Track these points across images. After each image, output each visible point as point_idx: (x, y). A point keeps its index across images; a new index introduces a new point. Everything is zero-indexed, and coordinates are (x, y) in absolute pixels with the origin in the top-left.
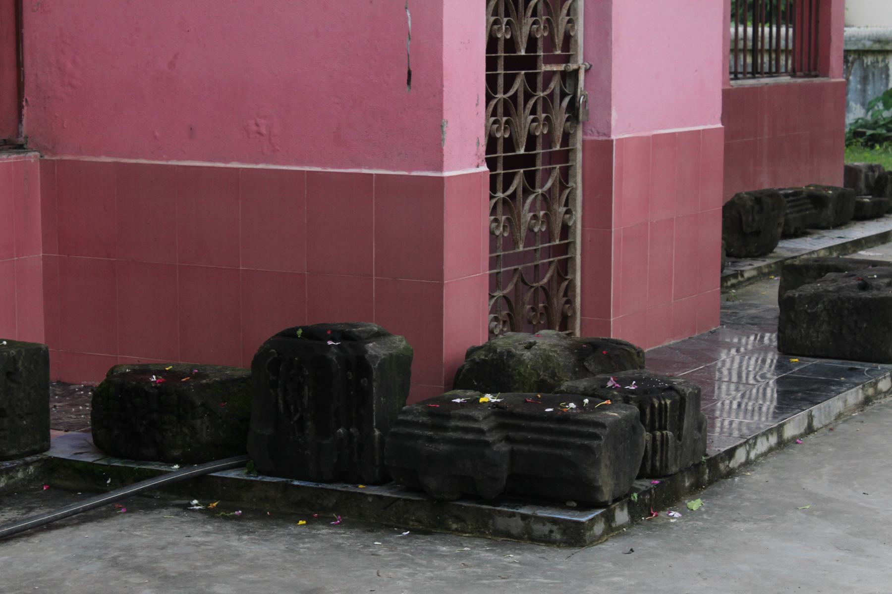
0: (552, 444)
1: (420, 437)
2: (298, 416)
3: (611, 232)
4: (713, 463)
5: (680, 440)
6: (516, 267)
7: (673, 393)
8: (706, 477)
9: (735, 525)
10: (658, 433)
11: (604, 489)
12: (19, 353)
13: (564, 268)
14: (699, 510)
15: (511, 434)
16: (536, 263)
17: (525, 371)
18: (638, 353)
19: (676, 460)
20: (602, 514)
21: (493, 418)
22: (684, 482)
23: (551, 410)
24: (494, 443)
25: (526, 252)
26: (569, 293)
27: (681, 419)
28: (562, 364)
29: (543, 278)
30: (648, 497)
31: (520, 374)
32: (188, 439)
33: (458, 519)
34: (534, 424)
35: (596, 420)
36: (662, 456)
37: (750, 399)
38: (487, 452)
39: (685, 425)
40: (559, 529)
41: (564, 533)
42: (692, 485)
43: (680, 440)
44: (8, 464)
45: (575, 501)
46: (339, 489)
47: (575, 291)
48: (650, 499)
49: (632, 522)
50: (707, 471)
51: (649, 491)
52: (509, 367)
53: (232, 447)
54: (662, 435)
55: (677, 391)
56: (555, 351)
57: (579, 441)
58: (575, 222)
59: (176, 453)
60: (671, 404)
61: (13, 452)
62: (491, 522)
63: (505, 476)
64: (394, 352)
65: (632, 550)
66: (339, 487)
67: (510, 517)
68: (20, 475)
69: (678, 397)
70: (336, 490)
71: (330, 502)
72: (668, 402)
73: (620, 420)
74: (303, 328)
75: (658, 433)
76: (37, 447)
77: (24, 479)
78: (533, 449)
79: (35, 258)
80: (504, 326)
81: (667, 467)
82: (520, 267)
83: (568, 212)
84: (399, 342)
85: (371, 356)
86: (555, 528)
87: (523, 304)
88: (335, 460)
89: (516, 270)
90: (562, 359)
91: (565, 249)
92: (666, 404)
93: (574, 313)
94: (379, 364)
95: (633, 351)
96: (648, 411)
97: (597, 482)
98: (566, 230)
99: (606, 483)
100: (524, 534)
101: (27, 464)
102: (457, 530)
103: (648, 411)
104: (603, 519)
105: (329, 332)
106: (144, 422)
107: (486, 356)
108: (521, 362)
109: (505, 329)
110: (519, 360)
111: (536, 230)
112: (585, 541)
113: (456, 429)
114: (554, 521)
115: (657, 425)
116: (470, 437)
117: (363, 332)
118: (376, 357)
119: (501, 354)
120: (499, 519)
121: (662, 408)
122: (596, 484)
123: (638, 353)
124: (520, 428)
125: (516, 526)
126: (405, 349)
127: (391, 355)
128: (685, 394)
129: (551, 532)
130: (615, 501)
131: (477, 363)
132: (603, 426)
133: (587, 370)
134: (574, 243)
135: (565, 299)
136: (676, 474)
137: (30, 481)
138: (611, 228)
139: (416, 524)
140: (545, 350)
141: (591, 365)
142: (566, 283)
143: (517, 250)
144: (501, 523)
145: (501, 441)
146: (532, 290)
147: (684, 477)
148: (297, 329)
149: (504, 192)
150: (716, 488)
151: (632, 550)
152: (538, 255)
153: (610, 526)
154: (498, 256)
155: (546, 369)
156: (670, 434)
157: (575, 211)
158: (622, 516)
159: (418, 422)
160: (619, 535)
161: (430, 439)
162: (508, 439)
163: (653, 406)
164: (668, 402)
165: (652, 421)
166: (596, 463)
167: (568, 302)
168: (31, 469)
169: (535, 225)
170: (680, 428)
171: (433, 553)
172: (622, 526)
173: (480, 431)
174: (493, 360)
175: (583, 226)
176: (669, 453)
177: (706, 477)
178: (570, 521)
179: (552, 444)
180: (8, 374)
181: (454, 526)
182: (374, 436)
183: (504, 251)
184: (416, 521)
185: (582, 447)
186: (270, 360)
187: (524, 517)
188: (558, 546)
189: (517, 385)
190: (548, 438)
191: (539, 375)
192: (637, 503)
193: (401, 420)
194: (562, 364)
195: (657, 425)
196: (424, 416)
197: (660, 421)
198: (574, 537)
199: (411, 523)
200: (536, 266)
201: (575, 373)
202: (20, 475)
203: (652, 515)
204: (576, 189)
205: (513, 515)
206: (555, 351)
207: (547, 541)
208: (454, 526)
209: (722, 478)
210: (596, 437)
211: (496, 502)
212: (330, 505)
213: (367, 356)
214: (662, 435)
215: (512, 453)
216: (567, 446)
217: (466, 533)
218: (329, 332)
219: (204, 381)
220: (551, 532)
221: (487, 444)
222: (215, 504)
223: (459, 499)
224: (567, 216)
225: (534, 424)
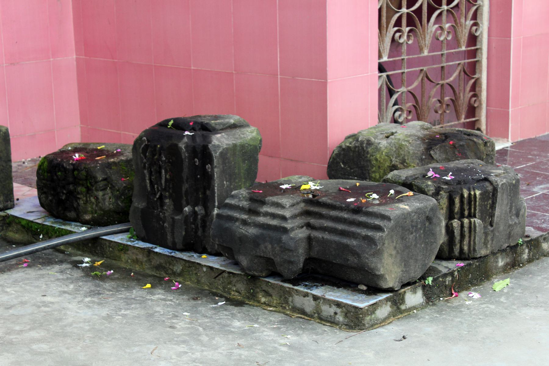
0: (343, 233)
1: (237, 219)
2: (159, 194)
3: (510, 40)
4: (534, 244)
5: (492, 226)
6: (421, 68)
7: (487, 184)
8: (525, 256)
9: (525, 310)
10: (466, 221)
11: (387, 276)
13: (472, 69)
14: (502, 291)
15: (313, 221)
16: (442, 65)
17: (380, 157)
18: (485, 144)
19: (485, 244)
20: (387, 299)
21: (302, 205)
22: (497, 262)
23: (352, 200)
24: (292, 229)
25: (430, 56)
26: (477, 89)
27: (493, 206)
28: (411, 152)
29: (451, 77)
30: (449, 279)
31: (376, 160)
32: (94, 206)
33: (267, 294)
34: (333, 213)
35: (383, 213)
36: (470, 241)
37: (462, 216)
38: (284, 238)
39: (497, 212)
40: (342, 312)
41: (346, 316)
42: (507, 265)
43: (492, 226)
45: (365, 285)
46: (185, 258)
47: (481, 87)
48: (452, 281)
49: (427, 303)
50: (527, 251)
51: (452, 274)
52: (368, 153)
53: (118, 216)
54: (470, 222)
55: (491, 183)
56: (408, 141)
57: (364, 232)
58: (482, 33)
59: (87, 217)
60: (481, 194)
62: (290, 299)
63: (302, 259)
64: (238, 142)
65: (404, 337)
66: (184, 256)
67: (304, 297)
69: (490, 188)
70: (182, 259)
71: (178, 268)
72: (478, 193)
73: (409, 214)
74: (175, 120)
75: (466, 221)
78: (327, 236)
79: (70, 59)
80: (408, 115)
81: (474, 250)
82: (425, 68)
83: (476, 24)
84: (250, 134)
85: (214, 145)
86: (339, 310)
87: (430, 97)
88: (184, 233)
89: (422, 70)
90: (414, 148)
91: (473, 54)
92: (475, 194)
93: (480, 104)
94: (221, 153)
95: (480, 142)
96: (457, 201)
97: (379, 271)
98: (473, 39)
99: (390, 270)
100: (315, 313)
102: (265, 303)
103: (457, 201)
104: (389, 303)
105: (191, 124)
106: (65, 192)
107: (350, 144)
108: (377, 149)
109: (410, 118)
110: (376, 148)
111: (442, 39)
112: (364, 325)
113: (266, 214)
114: (339, 305)
115: (466, 213)
116: (274, 222)
117: (220, 124)
118: (218, 146)
119: (362, 142)
120: (296, 297)
121: (471, 199)
122: (377, 273)
123: (485, 144)
124: (321, 216)
125: (309, 305)
126: (253, 139)
127: (235, 145)
128: (498, 185)
129: (336, 313)
130: (404, 286)
131: (344, 149)
132: (388, 218)
133: (433, 158)
134: (481, 49)
135: (472, 93)
136: (486, 256)
138: (510, 37)
139: (237, 294)
140: (399, 139)
141: (436, 153)
142: (473, 81)
143: (422, 55)
144: (298, 301)
145: (302, 227)
146: (438, 86)
147: (497, 258)
148: (170, 120)
149: (407, 8)
150: (532, 267)
151: (404, 337)
152: (444, 59)
153: (398, 308)
154: (403, 59)
155: (398, 155)
156: (477, 221)
157: (482, 23)
158: (413, 298)
159: (239, 206)
160: (409, 316)
161: (245, 223)
162: (309, 226)
163: (462, 196)
164: (478, 193)
165: (462, 209)
166: (378, 253)
167: (475, 95)
169: (441, 35)
170: (492, 216)
171: (225, 330)
172: (414, 308)
173: (284, 218)
174: (356, 147)
175: (489, 35)
176: (477, 239)
177: (525, 256)
178: (351, 306)
179: (343, 233)
181: (263, 300)
182: (213, 215)
183: (407, 55)
184: (237, 291)
185: (366, 238)
186: (143, 146)
187: (315, 298)
188: (340, 328)
189: (374, 169)
190: (340, 227)
191: (391, 161)
192: (433, 286)
193: (227, 204)
194: (411, 152)
195: (466, 213)
196: (246, 201)
197: (470, 209)
198: (355, 321)
199: (233, 293)
200: (442, 67)
201: (422, 160)
203: (452, 294)
204: (483, 6)
205: (306, 295)
206: (408, 141)
207: (331, 322)
208: (263, 300)
209: (545, 256)
210: (378, 228)
211: (295, 282)
212: (179, 271)
213: (210, 146)
214: (470, 222)
215: (309, 239)
216: (353, 235)
217: (271, 306)
218: (191, 124)
219: (112, 160)
220: (336, 313)
221: (285, 231)
222: (99, 263)
223: (267, 277)
224: (474, 28)
225: (333, 213)
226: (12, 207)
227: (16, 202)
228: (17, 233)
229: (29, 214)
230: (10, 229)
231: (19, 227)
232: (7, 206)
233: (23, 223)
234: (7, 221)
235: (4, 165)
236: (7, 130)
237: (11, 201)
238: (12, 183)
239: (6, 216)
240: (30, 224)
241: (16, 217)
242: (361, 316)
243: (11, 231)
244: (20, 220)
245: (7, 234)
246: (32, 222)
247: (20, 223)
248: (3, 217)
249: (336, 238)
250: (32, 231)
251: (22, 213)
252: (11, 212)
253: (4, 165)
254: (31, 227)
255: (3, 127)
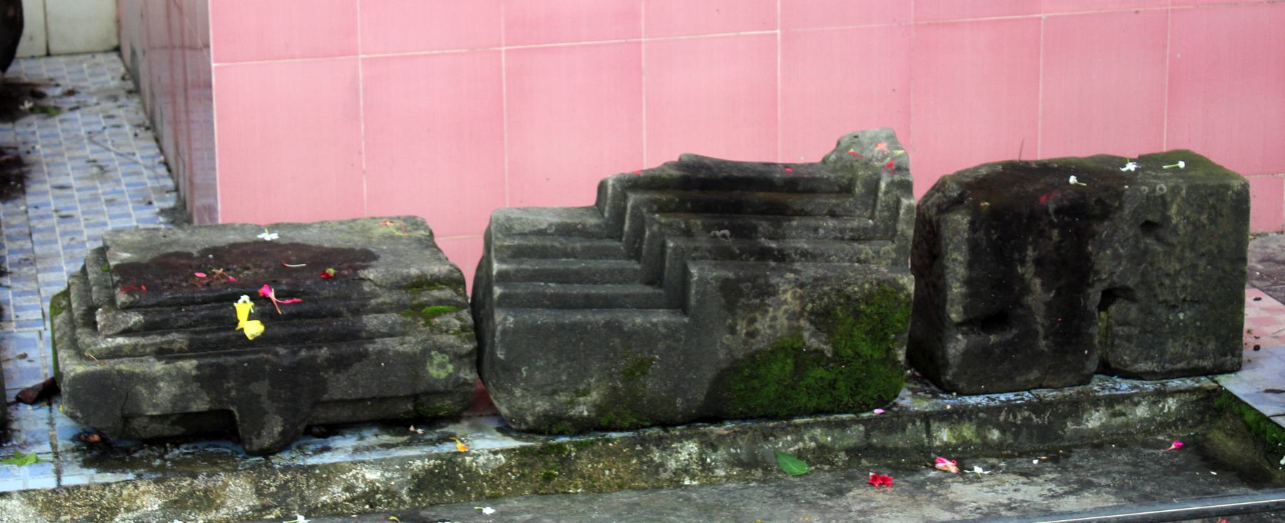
12: (1175, 190)
44: (1124, 386)
61: (1143, 366)
68: (1142, 411)
76: (1206, 363)
77: (1141, 421)
101: (1162, 394)
137: (1164, 426)
168: (1171, 404)
180: (1148, 227)
202: (1142, 411)
214: (508, 302)
226: (1235, 368)
227: (1247, 353)
228: (1232, 436)
229: (1269, 395)
230: (1220, 423)
231: (1239, 422)
232: (1223, 364)
233: (1249, 417)
234: (1217, 403)
235: (1228, 267)
236: (1245, 187)
237: (1233, 355)
238: (1243, 287)
239: (1214, 390)
240: (1262, 424)
241: (1236, 399)
242: (867, 286)
243: (1220, 429)
244: (1243, 407)
245: (1211, 436)
246: (1268, 420)
247: (1241, 415)
248: (1208, 391)
249: (599, 317)
250: (1265, 442)
251: (1254, 391)
252: (1230, 383)
253: (1228, 267)
254: (1265, 432)
255: (1237, 177)
